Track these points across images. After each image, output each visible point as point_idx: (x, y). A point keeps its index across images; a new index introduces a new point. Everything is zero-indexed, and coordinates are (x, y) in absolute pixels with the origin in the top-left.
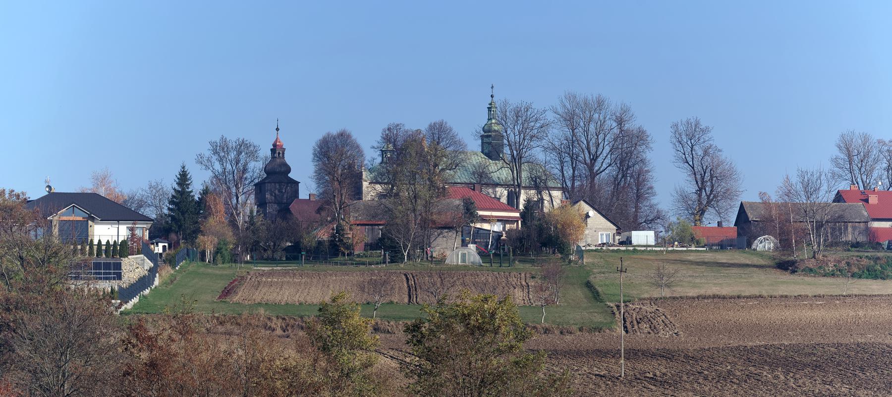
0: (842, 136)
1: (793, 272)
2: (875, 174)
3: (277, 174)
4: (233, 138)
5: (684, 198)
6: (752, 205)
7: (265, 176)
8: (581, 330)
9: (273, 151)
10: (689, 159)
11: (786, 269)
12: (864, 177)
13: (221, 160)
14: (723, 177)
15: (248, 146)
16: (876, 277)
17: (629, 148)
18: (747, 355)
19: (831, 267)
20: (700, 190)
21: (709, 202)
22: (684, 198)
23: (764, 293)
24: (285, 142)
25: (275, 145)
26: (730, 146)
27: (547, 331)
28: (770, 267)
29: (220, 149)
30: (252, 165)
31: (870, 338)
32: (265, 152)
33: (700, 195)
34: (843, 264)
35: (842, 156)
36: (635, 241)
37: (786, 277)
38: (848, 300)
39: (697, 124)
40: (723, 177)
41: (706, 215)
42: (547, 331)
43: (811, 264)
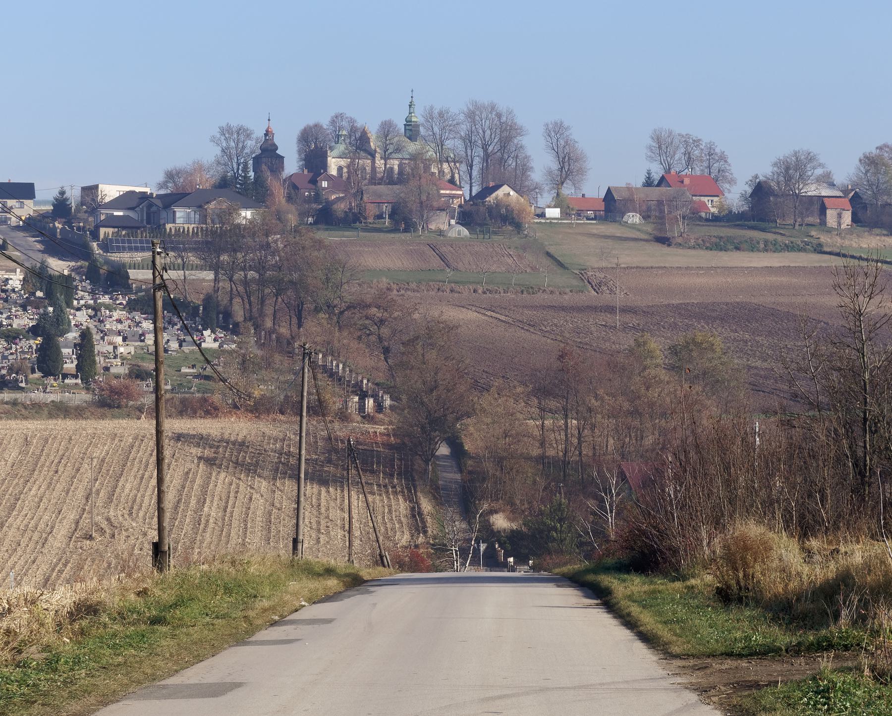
0: (655, 130)
1: (669, 245)
2: (677, 157)
3: (269, 154)
4: (234, 123)
5: (550, 172)
6: (616, 188)
7: (260, 151)
8: (571, 291)
9: (266, 135)
10: (878, 325)
11: (664, 243)
12: (669, 159)
13: (226, 139)
14: (577, 160)
15: (245, 130)
16: (721, 250)
17: (507, 133)
18: (679, 310)
19: (692, 243)
20: (562, 168)
21: (567, 176)
22: (550, 172)
23: (667, 265)
24: (274, 129)
25: (267, 131)
26: (583, 138)
27: (552, 293)
28: (646, 240)
29: (226, 131)
30: (249, 143)
31: (740, 298)
32: (260, 133)
33: (561, 172)
34: (700, 241)
35: (654, 144)
36: (547, 215)
37: (665, 249)
38: (718, 270)
39: (562, 123)
40: (577, 160)
41: (565, 185)
42: (552, 293)
43: (680, 240)
